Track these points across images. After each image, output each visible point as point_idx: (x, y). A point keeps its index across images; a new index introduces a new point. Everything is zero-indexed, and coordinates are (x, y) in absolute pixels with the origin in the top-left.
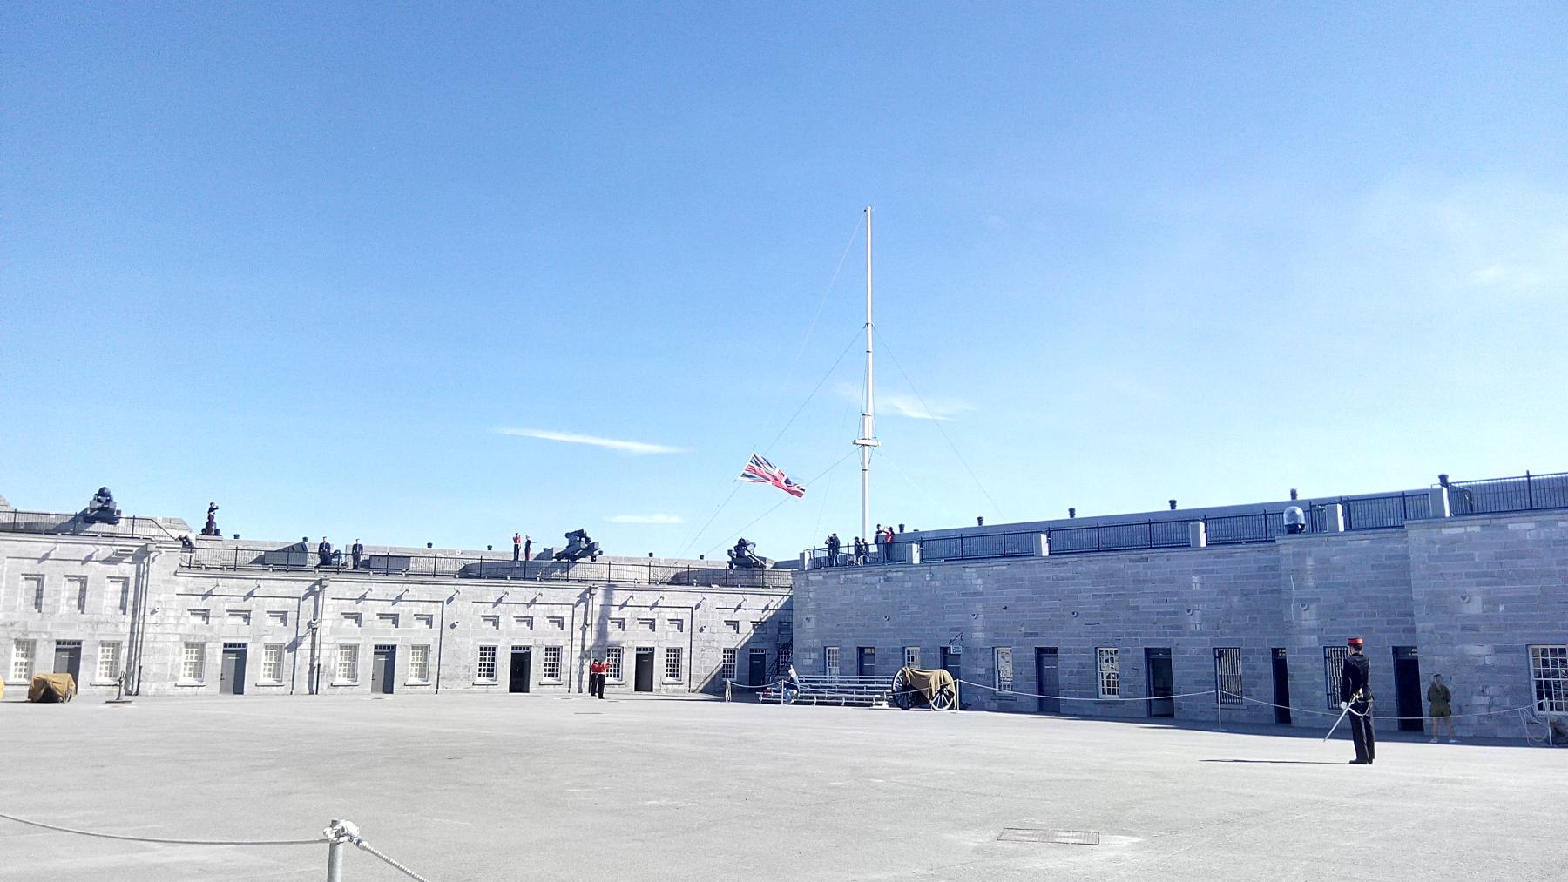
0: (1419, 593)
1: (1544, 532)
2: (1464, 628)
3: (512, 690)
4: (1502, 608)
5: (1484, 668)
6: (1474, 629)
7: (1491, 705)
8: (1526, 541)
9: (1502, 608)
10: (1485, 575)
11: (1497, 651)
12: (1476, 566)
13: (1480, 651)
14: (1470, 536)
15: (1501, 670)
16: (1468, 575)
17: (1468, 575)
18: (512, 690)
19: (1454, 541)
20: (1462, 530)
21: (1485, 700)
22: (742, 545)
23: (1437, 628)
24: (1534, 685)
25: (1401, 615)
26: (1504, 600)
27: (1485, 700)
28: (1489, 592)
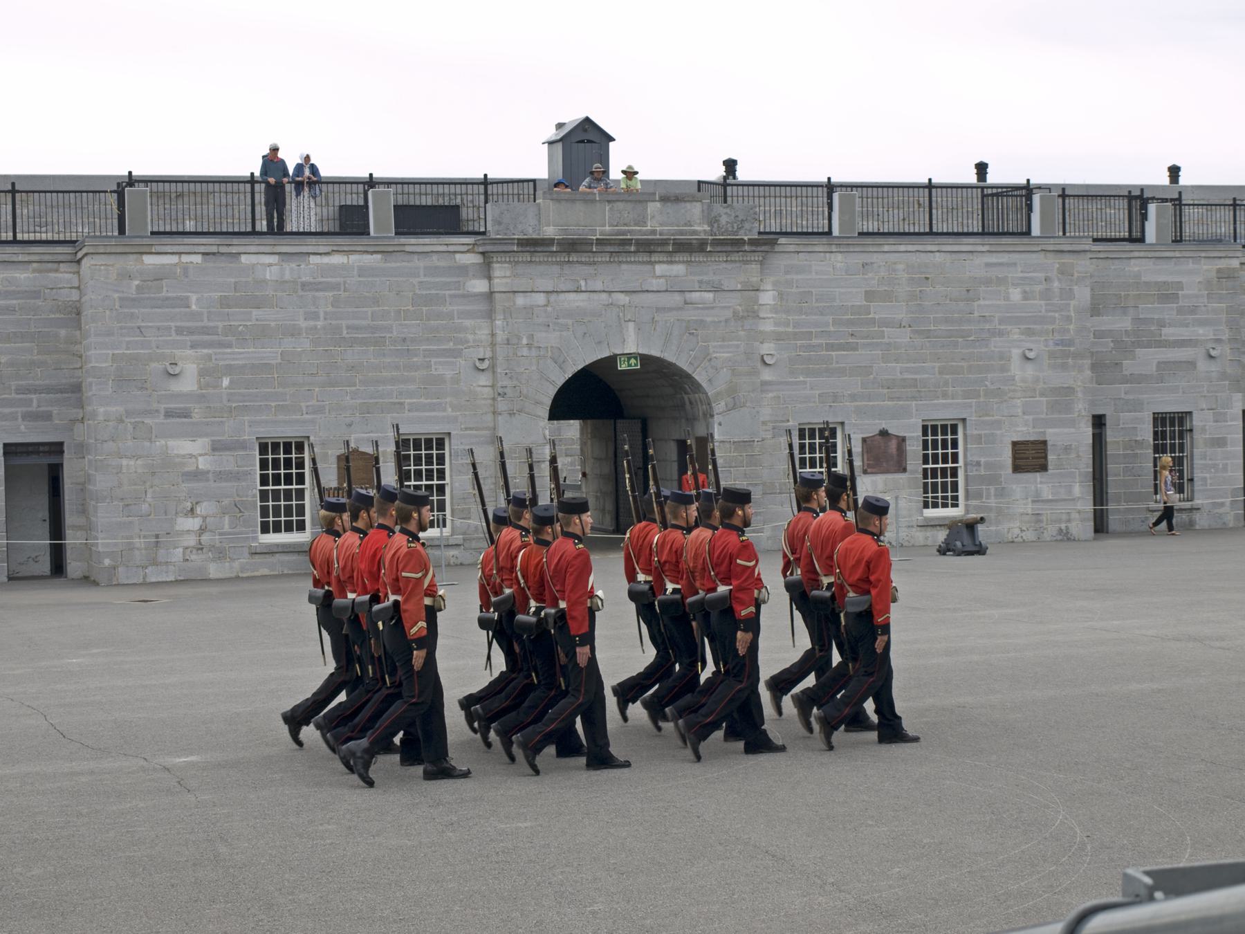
0: (99, 355)
1: (290, 270)
2: (169, 414)
3: (5, 445)
4: (226, 382)
5: (197, 475)
6: (186, 414)
7: (202, 530)
8: (265, 281)
9: (226, 382)
10: (205, 331)
11: (216, 448)
12: (195, 316)
13: (191, 449)
14: (185, 269)
15: (220, 476)
16: (179, 331)
17: (179, 331)
18: (5, 445)
19: (159, 276)
20: (174, 259)
21: (193, 524)
22: (275, 150)
23: (129, 413)
24: (961, 473)
25: (19, 391)
26: (229, 370)
27: (193, 524)
28: (209, 357)
